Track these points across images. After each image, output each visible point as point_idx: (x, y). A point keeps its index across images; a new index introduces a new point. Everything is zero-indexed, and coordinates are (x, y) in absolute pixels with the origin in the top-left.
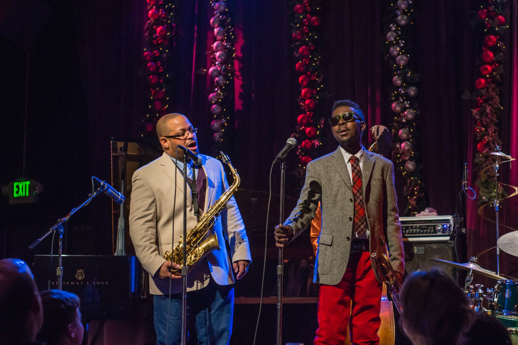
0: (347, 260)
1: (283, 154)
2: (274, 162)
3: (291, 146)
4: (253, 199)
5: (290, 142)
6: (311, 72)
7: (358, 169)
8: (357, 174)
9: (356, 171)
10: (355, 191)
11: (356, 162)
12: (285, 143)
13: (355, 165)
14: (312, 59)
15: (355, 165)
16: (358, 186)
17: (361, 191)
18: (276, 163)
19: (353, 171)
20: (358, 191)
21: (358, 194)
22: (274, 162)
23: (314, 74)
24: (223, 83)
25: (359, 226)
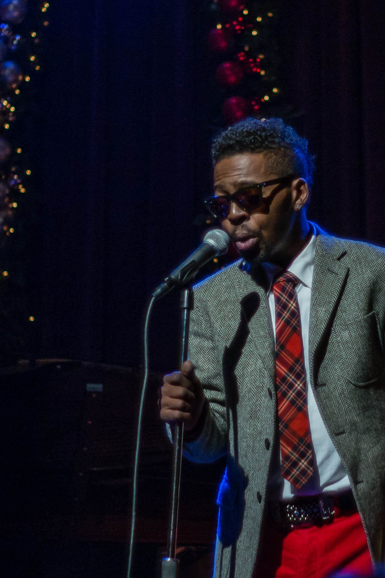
0: (254, 552)
1: (183, 273)
2: (159, 290)
3: (212, 251)
4: (90, 387)
5: (211, 242)
6: (248, 55)
7: (292, 305)
8: (287, 322)
9: (286, 315)
10: (283, 370)
11: (289, 287)
12: (198, 241)
13: (284, 298)
14: (249, 21)
15: (284, 298)
16: (291, 355)
17: (298, 368)
18: (161, 294)
19: (279, 315)
20: (291, 369)
21: (291, 378)
22: (159, 290)
23: (255, 58)
24: (16, 81)
25: (295, 464)
